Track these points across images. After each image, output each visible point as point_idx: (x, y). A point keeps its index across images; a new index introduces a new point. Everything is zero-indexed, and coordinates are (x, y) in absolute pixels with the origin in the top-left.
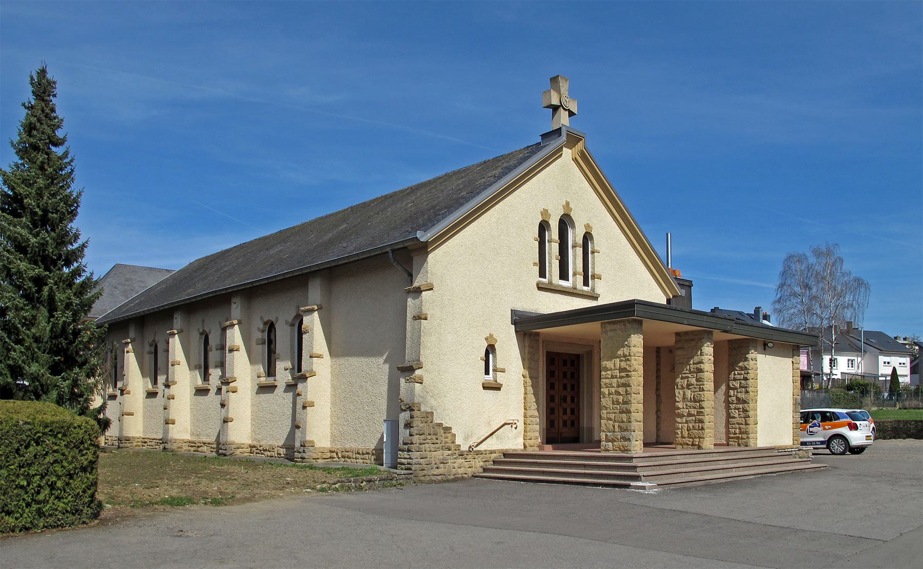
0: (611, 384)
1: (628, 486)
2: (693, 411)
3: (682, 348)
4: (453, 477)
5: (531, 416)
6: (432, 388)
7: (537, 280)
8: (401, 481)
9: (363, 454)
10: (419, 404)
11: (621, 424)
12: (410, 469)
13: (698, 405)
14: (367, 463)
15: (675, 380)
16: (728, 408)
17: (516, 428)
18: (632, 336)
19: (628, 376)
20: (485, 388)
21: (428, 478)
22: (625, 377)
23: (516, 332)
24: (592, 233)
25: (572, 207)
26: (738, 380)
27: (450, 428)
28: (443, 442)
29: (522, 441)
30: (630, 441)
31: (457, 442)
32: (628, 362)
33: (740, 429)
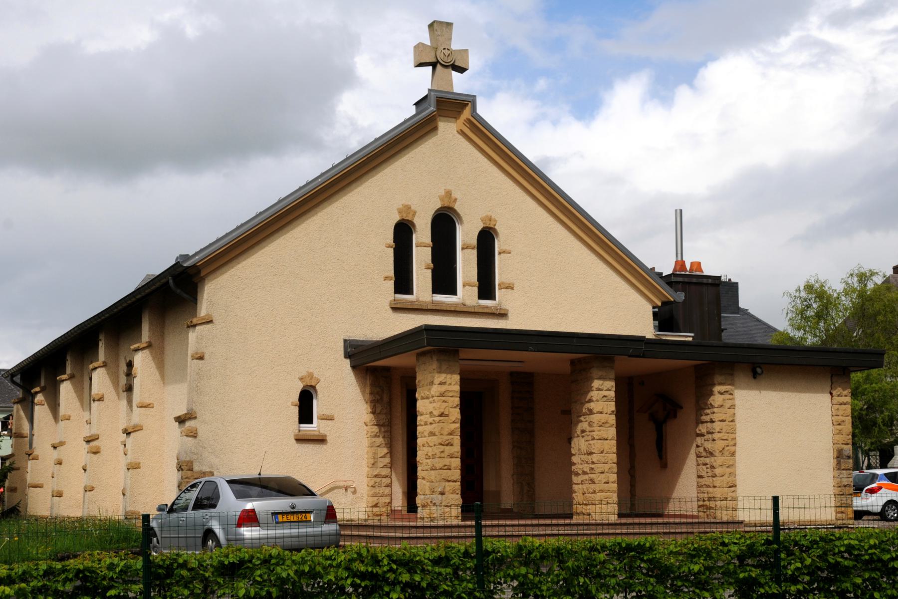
23: (354, 367)
24: (496, 227)
25: (458, 197)
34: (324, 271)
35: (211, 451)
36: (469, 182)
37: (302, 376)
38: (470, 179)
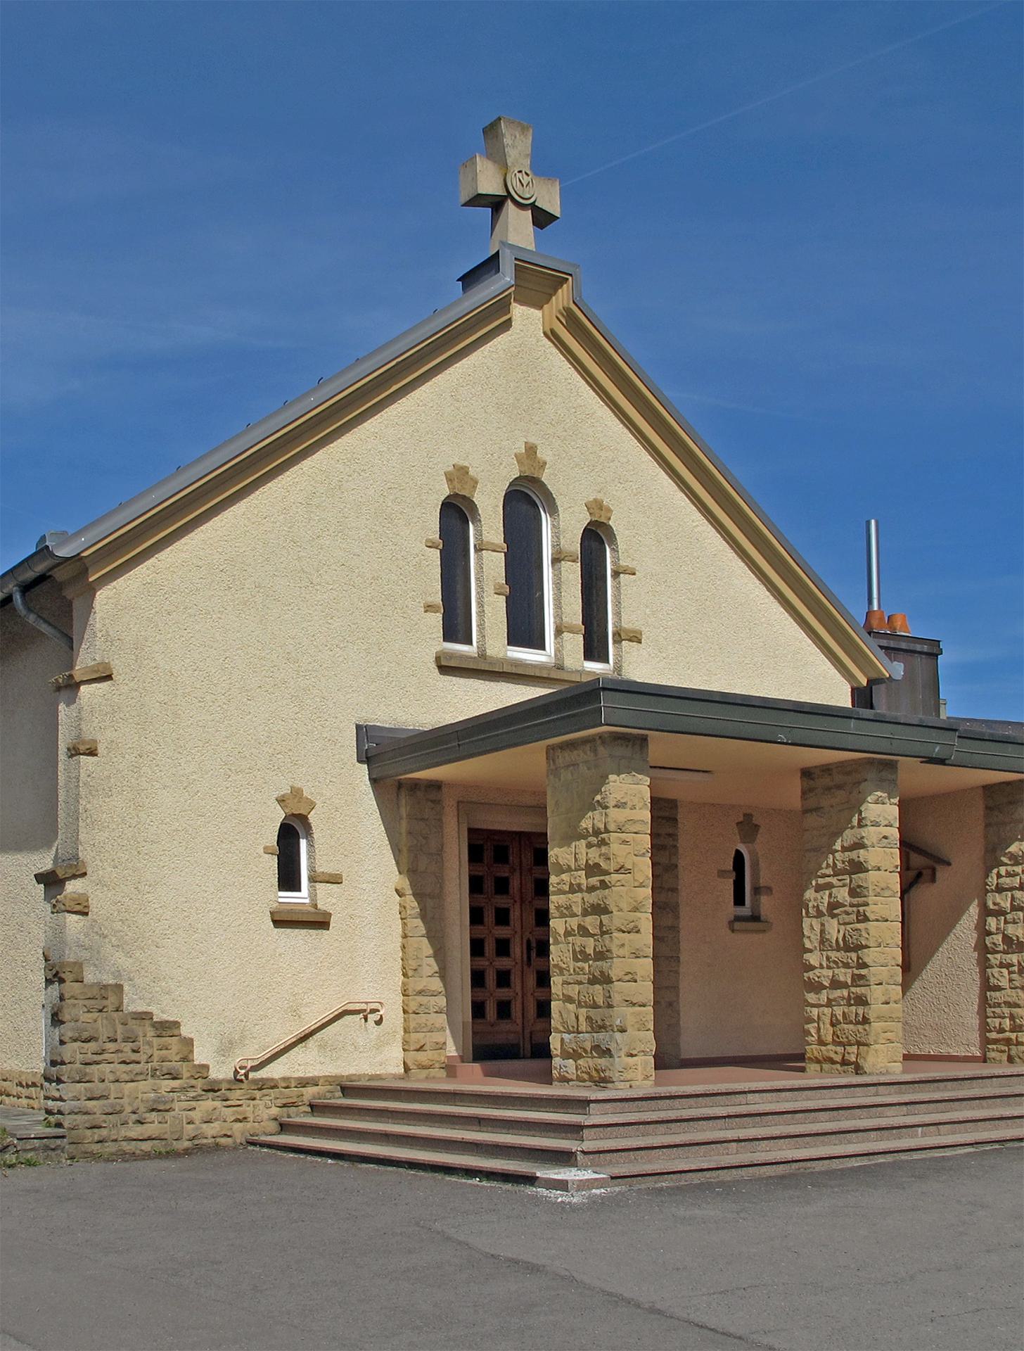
0: (569, 908)
1: (530, 1180)
2: (844, 975)
3: (817, 809)
4: (187, 1144)
5: (420, 993)
6: (118, 925)
7: (439, 648)
8: (29, 1155)
9: (28, 1086)
10: (79, 965)
11: (592, 1012)
12: (59, 1125)
13: (855, 959)
14: (33, 1108)
15: (802, 895)
16: (984, 965)
17: (379, 1022)
18: (612, 777)
19: (604, 885)
20: (278, 923)
21: (110, 1148)
22: (597, 889)
23: (374, 781)
24: (611, 523)
25: (548, 459)
26: (1007, 890)
27: (176, 1024)
28: (155, 1058)
29: (400, 1054)
30: (611, 1056)
31: (199, 1057)
32: (604, 849)
33: (1012, 1017)
34: (318, 587)
35: (115, 943)
36: (565, 433)
37: (283, 796)
38: (566, 427)
